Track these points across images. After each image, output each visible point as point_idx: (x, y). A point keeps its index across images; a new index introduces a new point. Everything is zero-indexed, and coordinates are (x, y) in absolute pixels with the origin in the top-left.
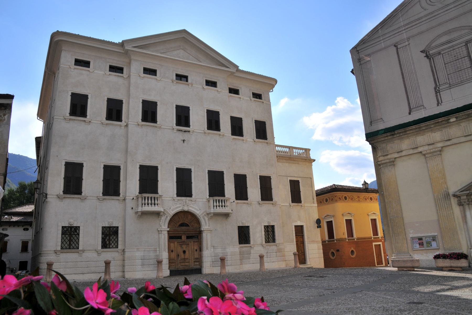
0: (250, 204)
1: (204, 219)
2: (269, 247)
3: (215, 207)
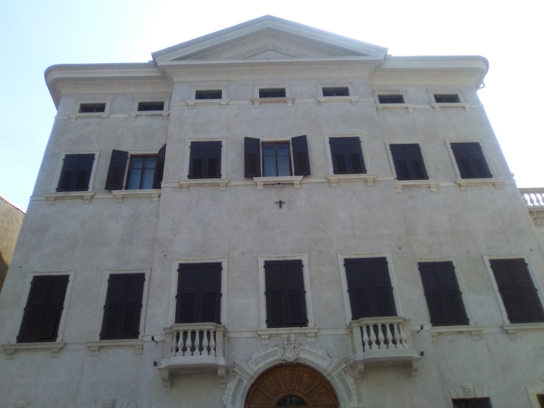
0: (479, 335)
1: (343, 381)
3: (367, 345)
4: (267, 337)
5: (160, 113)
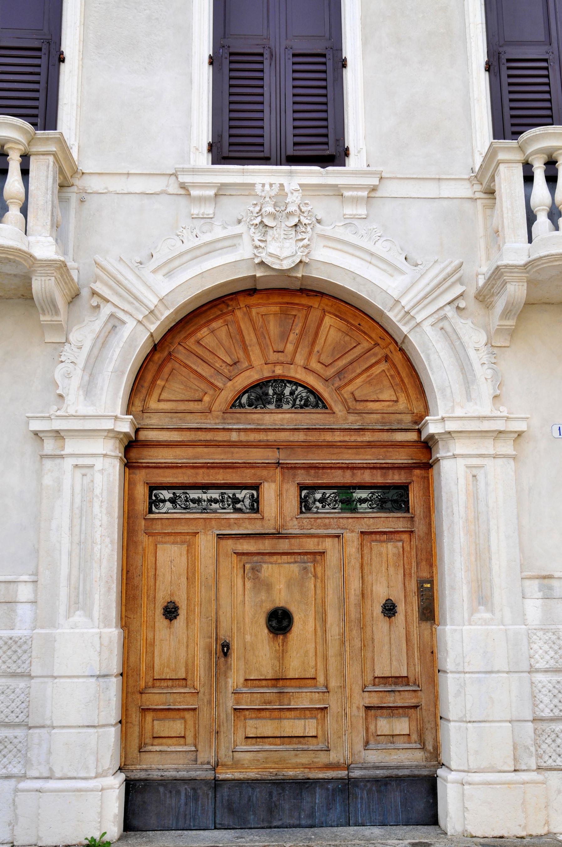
3: (542, 220)
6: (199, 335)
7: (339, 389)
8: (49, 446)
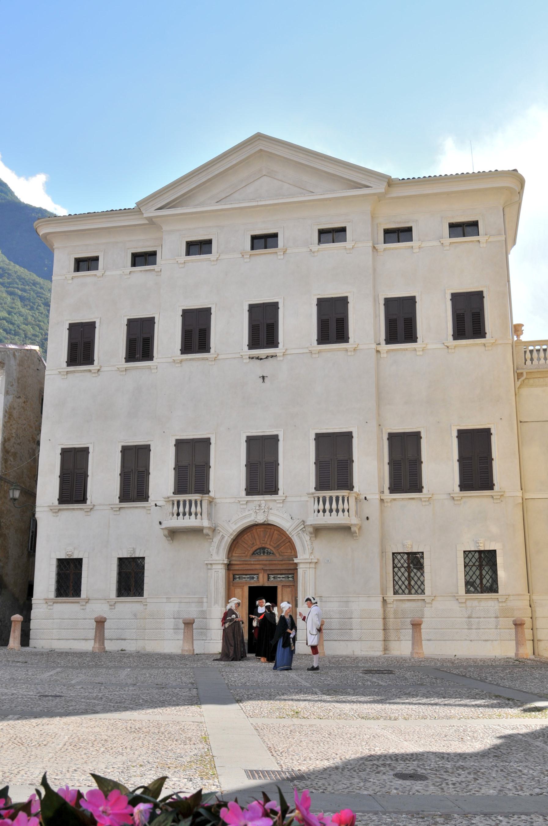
1: (300, 538)
2: (475, 603)
4: (245, 503)
5: (153, 269)
6: (244, 537)
7: (278, 550)
8: (209, 566)
